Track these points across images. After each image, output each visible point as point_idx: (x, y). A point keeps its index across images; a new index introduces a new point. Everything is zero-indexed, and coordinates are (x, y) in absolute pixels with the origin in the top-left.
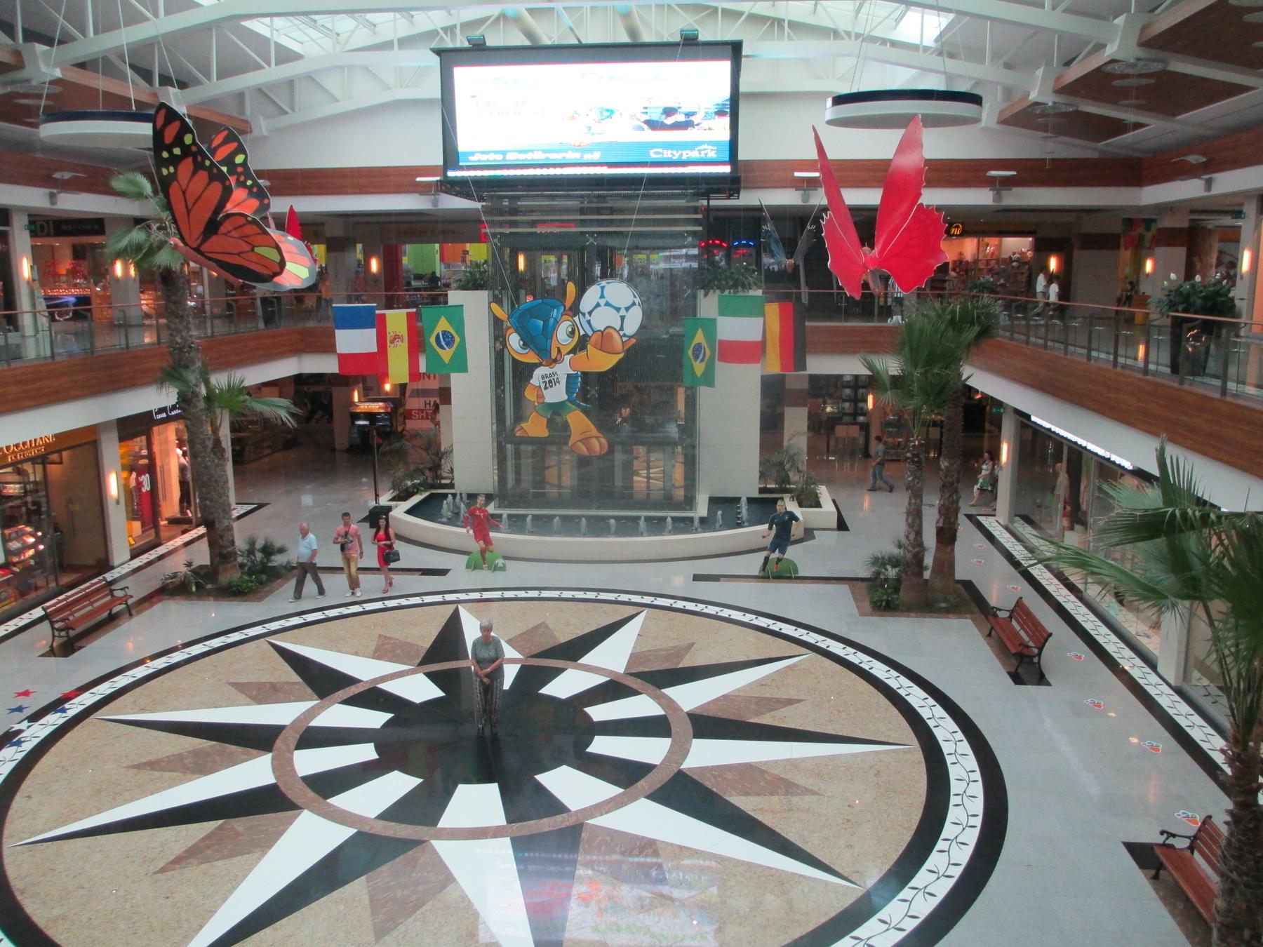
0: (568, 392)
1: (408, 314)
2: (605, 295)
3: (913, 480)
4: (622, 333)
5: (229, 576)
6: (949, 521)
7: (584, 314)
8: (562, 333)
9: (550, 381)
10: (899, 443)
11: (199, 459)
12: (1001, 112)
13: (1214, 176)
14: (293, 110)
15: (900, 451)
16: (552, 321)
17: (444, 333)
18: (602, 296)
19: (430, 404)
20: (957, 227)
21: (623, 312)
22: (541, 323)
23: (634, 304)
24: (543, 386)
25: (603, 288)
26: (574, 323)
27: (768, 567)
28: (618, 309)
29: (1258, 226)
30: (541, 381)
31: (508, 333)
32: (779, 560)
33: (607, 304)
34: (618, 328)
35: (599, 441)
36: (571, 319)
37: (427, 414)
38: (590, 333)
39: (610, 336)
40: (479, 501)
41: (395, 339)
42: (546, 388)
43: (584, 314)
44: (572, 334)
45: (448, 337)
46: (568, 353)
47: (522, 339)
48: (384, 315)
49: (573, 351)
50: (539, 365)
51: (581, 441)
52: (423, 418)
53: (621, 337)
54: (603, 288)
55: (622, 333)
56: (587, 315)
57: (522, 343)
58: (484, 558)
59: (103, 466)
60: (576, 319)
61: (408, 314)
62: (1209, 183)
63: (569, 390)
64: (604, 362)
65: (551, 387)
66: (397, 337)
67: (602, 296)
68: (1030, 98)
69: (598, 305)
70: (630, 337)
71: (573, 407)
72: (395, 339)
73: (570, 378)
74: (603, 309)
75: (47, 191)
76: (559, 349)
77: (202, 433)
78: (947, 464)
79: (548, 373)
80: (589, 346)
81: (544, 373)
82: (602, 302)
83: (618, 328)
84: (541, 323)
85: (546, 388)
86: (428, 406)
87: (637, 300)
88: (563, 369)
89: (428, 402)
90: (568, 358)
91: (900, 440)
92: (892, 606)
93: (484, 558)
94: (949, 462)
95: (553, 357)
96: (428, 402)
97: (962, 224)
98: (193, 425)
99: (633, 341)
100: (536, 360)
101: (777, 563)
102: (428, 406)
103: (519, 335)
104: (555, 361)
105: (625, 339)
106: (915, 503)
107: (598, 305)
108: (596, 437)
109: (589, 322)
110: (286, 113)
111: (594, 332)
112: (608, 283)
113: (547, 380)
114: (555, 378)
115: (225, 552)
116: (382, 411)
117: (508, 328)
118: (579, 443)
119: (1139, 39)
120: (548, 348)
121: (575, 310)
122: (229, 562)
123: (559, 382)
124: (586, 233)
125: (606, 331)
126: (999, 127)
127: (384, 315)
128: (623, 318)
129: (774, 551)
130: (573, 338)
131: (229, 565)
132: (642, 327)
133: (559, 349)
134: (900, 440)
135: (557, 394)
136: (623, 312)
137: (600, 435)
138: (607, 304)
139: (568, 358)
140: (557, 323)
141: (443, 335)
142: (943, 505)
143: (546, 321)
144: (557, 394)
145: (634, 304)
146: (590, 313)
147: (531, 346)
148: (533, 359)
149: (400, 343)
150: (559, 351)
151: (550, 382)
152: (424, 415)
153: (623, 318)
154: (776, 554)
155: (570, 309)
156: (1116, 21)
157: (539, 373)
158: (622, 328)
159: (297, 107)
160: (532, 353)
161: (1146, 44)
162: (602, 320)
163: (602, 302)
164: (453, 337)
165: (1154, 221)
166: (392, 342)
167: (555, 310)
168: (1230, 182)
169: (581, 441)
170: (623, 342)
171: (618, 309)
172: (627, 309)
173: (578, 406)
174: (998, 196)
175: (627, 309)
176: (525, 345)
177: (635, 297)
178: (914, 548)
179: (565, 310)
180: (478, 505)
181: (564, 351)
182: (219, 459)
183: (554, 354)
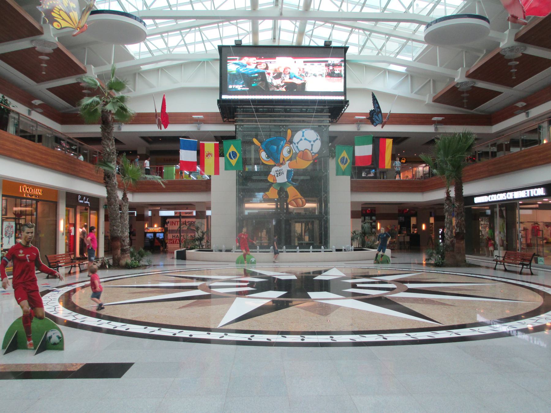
0: (287, 178)
1: (215, 144)
2: (304, 135)
3: (449, 207)
4: (312, 152)
5: (126, 260)
6: (462, 229)
7: (295, 144)
8: (285, 151)
9: (279, 173)
10: (394, 241)
11: (112, 206)
12: (434, 97)
13: (529, 111)
14: (135, 90)
15: (394, 245)
16: (280, 146)
17: (233, 152)
18: (303, 136)
19: (175, 236)
20: (404, 159)
21: (312, 143)
22: (275, 147)
23: (317, 139)
24: (276, 175)
25: (303, 132)
26: (290, 148)
27: (378, 258)
28: (310, 142)
29: (549, 130)
30: (275, 173)
31: (260, 152)
32: (382, 256)
33: (305, 139)
34: (310, 149)
35: (302, 200)
36: (289, 145)
37: (173, 241)
38: (298, 152)
39: (307, 153)
40: (243, 231)
41: (208, 155)
42: (277, 176)
43: (295, 144)
44: (289, 152)
45: (234, 154)
46: (288, 161)
47: (267, 154)
48: (204, 144)
49: (291, 159)
50: (275, 166)
51: (293, 200)
52: (171, 243)
53: (311, 153)
54: (303, 132)
55: (312, 152)
56: (296, 144)
57: (267, 156)
58: (245, 258)
59: (59, 215)
60: (291, 145)
61: (215, 144)
62: (527, 114)
63: (288, 177)
64: (304, 165)
65: (280, 175)
66: (209, 154)
67: (303, 136)
68: (455, 81)
69: (301, 140)
70: (316, 154)
71: (290, 185)
72: (208, 155)
73: (289, 172)
74: (303, 141)
75: (27, 108)
76: (283, 158)
77: (115, 194)
78: (458, 204)
79: (279, 169)
80: (297, 157)
81: (276, 169)
82: (303, 138)
83: (310, 149)
84: (275, 147)
85: (277, 176)
86: (174, 238)
87: (319, 137)
88: (285, 168)
89: (174, 236)
90: (287, 163)
91: (395, 240)
92: (444, 264)
93: (245, 258)
94: (459, 203)
95: (281, 162)
96: (174, 236)
97: (405, 158)
98: (111, 190)
99: (317, 155)
100: (273, 164)
101: (381, 257)
102: (174, 238)
103: (266, 152)
104: (282, 164)
105: (313, 154)
106: (450, 218)
107: (301, 140)
108: (301, 198)
109: (297, 147)
110: (131, 91)
111: (299, 151)
112: (306, 130)
113: (278, 172)
114: (282, 171)
115: (125, 248)
116: (160, 231)
117: (261, 149)
118: (292, 201)
119: (515, 38)
120: (279, 159)
121: (291, 142)
122: (127, 254)
123: (283, 173)
124: (281, 125)
125: (305, 151)
126: (433, 103)
127: (204, 144)
128: (312, 145)
129: (380, 251)
130: (290, 154)
131: (126, 255)
132: (321, 149)
133: (283, 158)
134: (395, 240)
135: (282, 179)
136: (312, 143)
137: (302, 197)
138: (305, 139)
139: (287, 163)
140: (283, 147)
141: (232, 153)
142: (458, 222)
143: (278, 146)
144: (282, 179)
145: (317, 139)
146: (298, 143)
147: (271, 157)
148: (271, 163)
149: (211, 157)
150: (284, 160)
151: (279, 173)
152: (172, 241)
153: (312, 145)
154: (381, 253)
155: (289, 141)
156: (505, 32)
157: (274, 169)
158: (312, 150)
159: (137, 89)
160: (272, 161)
161: (517, 40)
162: (303, 146)
163: (303, 138)
164: (236, 154)
165: (496, 143)
166: (207, 156)
167: (282, 142)
168: (535, 112)
169: (293, 200)
170: (312, 156)
171: (310, 142)
172: (314, 141)
173: (292, 184)
174: (436, 129)
175: (314, 141)
176: (268, 157)
177: (317, 136)
178: (450, 238)
179: (286, 142)
180: (243, 233)
181: (286, 160)
182: (125, 203)
183: (281, 161)
